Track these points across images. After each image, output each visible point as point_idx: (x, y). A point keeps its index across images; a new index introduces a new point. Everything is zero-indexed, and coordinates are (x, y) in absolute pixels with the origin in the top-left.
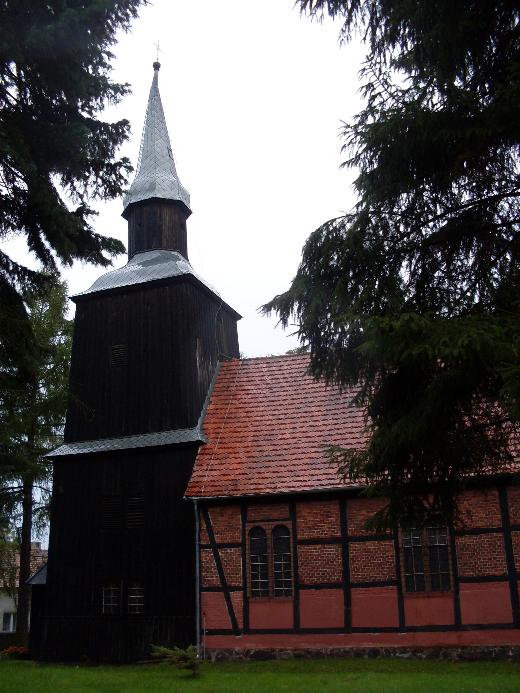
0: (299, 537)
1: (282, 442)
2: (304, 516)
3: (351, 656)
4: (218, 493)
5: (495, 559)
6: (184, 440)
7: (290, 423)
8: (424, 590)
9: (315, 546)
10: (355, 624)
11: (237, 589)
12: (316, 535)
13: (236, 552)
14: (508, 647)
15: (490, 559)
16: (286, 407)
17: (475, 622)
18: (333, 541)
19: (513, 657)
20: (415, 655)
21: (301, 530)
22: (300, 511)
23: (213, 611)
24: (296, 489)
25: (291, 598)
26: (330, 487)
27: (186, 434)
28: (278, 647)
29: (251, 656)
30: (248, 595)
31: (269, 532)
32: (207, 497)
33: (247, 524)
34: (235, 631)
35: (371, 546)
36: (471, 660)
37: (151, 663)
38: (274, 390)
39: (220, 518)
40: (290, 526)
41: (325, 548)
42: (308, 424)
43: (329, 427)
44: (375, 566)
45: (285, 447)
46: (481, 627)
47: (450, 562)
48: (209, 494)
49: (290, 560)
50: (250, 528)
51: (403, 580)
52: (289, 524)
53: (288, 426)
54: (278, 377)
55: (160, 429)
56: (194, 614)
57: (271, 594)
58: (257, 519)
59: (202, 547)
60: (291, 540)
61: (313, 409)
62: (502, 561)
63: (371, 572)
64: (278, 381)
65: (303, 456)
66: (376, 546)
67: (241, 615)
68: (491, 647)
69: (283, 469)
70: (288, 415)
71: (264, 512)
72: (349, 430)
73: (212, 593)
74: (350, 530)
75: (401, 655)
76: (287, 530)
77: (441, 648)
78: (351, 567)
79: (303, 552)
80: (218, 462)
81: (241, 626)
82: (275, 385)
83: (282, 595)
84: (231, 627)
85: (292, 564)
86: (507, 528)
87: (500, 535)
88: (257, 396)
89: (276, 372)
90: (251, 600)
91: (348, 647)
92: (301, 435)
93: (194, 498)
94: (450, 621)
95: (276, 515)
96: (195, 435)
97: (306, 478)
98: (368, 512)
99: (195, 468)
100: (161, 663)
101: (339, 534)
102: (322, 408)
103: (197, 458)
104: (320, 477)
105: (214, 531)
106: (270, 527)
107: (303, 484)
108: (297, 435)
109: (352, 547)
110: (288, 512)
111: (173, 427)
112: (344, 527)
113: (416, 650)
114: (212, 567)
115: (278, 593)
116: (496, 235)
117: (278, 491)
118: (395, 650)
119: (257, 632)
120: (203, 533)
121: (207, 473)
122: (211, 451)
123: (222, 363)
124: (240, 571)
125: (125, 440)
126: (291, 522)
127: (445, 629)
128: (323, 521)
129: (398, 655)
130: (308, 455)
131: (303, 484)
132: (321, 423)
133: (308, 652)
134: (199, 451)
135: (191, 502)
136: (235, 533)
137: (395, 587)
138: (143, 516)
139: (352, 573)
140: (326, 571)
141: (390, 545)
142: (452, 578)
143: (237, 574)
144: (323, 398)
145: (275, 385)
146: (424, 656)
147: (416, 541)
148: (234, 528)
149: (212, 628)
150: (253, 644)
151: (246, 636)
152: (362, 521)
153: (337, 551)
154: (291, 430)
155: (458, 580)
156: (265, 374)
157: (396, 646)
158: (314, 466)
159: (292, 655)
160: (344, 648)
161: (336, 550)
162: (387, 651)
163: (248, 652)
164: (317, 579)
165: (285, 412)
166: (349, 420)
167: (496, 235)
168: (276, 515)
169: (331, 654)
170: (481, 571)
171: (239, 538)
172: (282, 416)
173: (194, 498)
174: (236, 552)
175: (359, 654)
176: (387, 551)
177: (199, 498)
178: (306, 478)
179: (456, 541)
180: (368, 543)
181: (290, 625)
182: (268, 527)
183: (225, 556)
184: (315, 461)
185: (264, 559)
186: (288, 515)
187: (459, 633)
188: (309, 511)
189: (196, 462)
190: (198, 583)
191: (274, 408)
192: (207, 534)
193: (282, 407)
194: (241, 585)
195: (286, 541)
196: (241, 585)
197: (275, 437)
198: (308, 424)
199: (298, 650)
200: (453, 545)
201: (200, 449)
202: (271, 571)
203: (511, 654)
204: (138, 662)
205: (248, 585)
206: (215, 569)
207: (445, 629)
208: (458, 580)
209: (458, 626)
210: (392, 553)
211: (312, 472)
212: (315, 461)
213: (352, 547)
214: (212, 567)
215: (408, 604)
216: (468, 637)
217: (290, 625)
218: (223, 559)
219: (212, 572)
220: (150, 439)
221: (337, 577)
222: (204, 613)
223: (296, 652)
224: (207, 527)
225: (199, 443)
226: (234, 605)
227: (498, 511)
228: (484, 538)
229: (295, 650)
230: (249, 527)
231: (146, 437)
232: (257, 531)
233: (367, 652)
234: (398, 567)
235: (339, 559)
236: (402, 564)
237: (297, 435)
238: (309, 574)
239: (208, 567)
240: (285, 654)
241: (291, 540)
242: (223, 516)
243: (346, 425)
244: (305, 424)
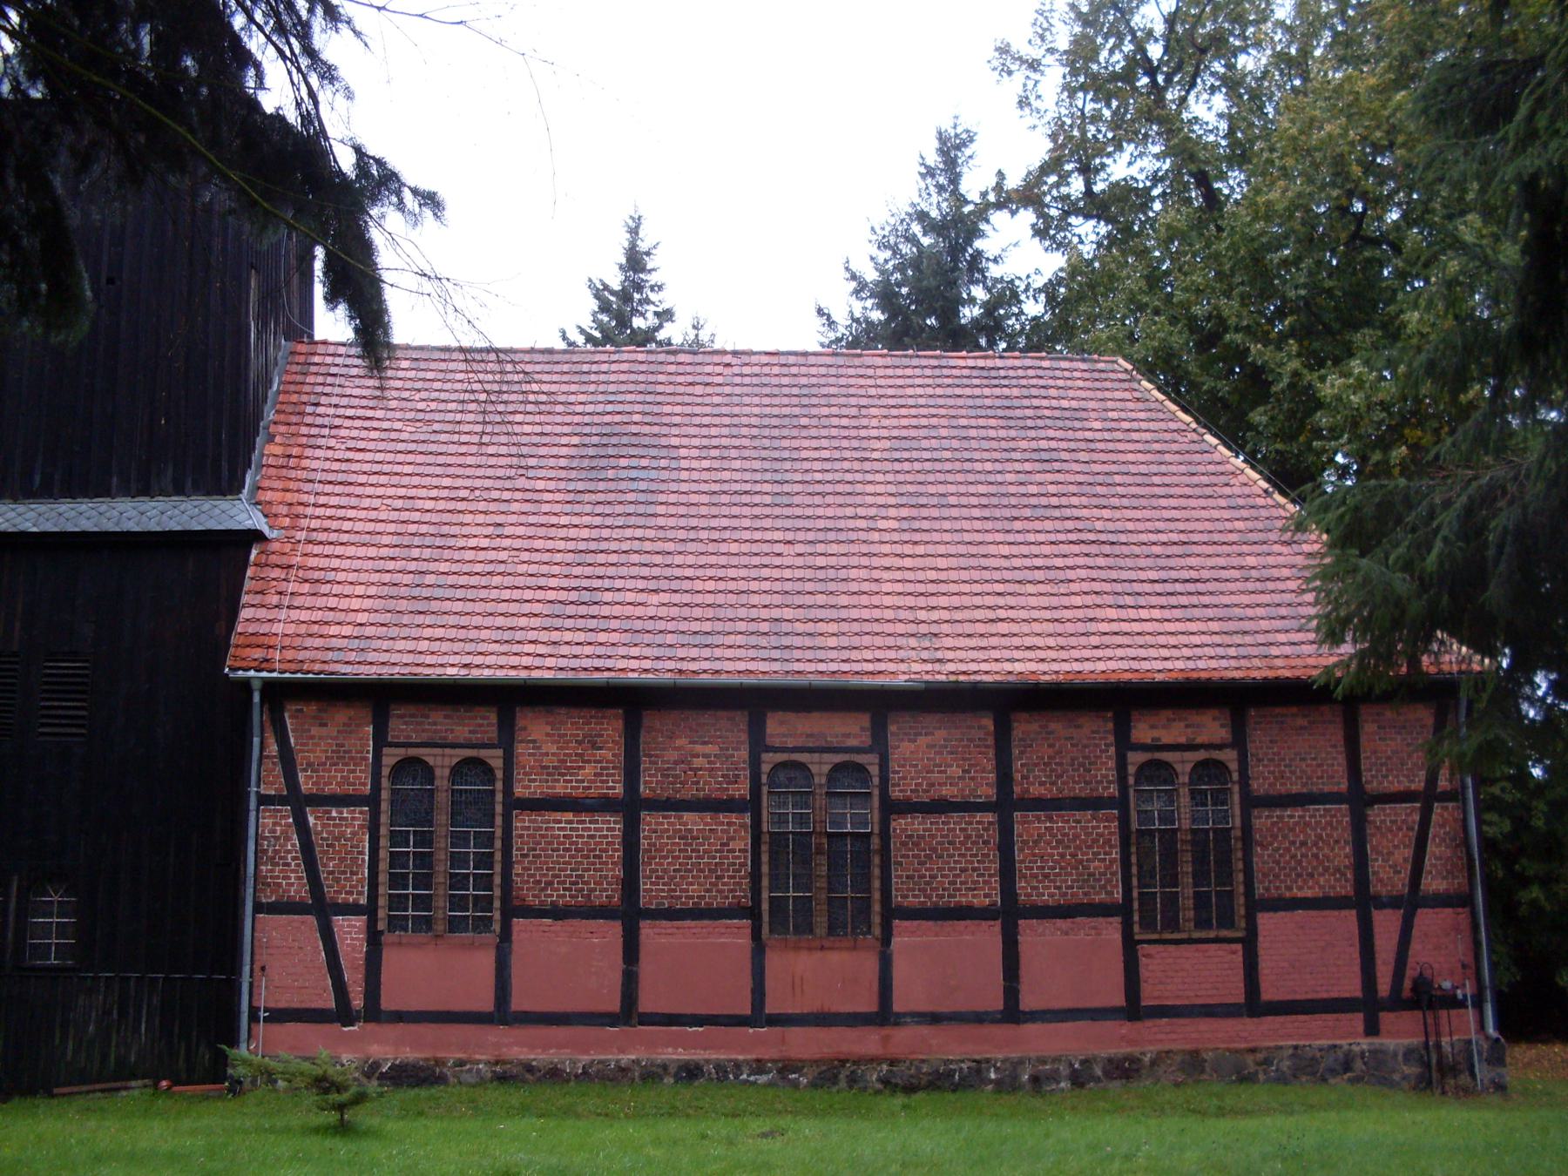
0: (519, 791)
1: (469, 555)
2: (534, 741)
3: (633, 1080)
4: (317, 667)
5: (974, 869)
6: (213, 525)
7: (485, 513)
8: (811, 931)
9: (558, 816)
10: (646, 1004)
11: (353, 909)
12: (560, 789)
13: (353, 819)
14: (988, 1061)
15: (963, 870)
16: (469, 472)
18: (605, 805)
19: (998, 1083)
21: (525, 774)
22: (525, 729)
23: (282, 960)
24: (523, 674)
25: (491, 938)
26: (606, 674)
27: (217, 511)
28: (453, 1056)
29: (382, 1077)
30: (381, 926)
31: (442, 774)
32: (287, 675)
33: (386, 750)
34: (343, 1014)
35: (695, 823)
36: (910, 1089)
37: (94, 1091)
38: (436, 427)
39: (314, 731)
40: (497, 763)
41: (583, 822)
42: (532, 519)
43: (585, 533)
44: (702, 871)
45: (478, 568)
46: (934, 1019)
48: (293, 666)
49: (492, 846)
50: (393, 761)
51: (765, 906)
52: (495, 758)
53: (480, 519)
54: (443, 396)
55: (145, 488)
56: (236, 969)
57: (440, 927)
58: (414, 739)
59: (264, 800)
60: (499, 797)
61: (540, 485)
62: (990, 876)
63: (692, 884)
64: (442, 406)
65: (528, 594)
66: (706, 824)
67: (360, 976)
68: (952, 1062)
69: (477, 620)
70: (477, 493)
71: (435, 724)
72: (636, 545)
73: (283, 918)
74: (646, 782)
75: (752, 1078)
76: (489, 771)
77: (843, 1062)
78: (645, 871)
79: (528, 828)
80: (306, 588)
81: (358, 1002)
82: (438, 417)
83: (466, 931)
84: (332, 1004)
85: (498, 856)
86: (1006, 804)
87: (990, 817)
88: (394, 435)
89: (437, 385)
90: (387, 938)
91: (626, 1058)
92: (518, 543)
93: (252, 673)
94: (868, 1004)
95: (462, 732)
96: (239, 514)
97: (541, 649)
98: (694, 743)
99: (245, 599)
100: (124, 1093)
101: (619, 790)
102: (562, 485)
103: (249, 573)
104: (577, 650)
105: (298, 761)
106: (447, 761)
107: (538, 662)
108: (507, 543)
109: (649, 824)
110: (495, 728)
111: (179, 489)
112: (631, 774)
113: (787, 1067)
114: (289, 852)
115: (454, 925)
117: (475, 673)
118: (738, 1066)
119: (399, 1017)
120: (268, 764)
121: (283, 614)
122: (284, 560)
123: (291, 345)
124: (362, 865)
125: (42, 508)
126: (500, 752)
128: (581, 755)
129: (744, 1076)
130: (540, 595)
131: (538, 662)
132: (564, 520)
133: (529, 1068)
134: (252, 557)
135: (246, 684)
136: (354, 771)
137: (747, 922)
138: (84, 713)
139: (644, 885)
140: (582, 876)
141: (741, 825)
142: (877, 907)
143: (352, 873)
144: (563, 463)
145: (438, 417)
146: (804, 1080)
147: (801, 819)
148: (352, 758)
149: (282, 1005)
150: (388, 1047)
151: (371, 1026)
152: (676, 763)
153: (613, 829)
154: (490, 530)
155: (891, 913)
156: (409, 385)
157: (741, 1057)
158: (558, 623)
159: (489, 1075)
160: (618, 1061)
161: (609, 827)
162: (721, 1068)
164: (554, 896)
165: (468, 483)
166: (632, 521)
168: (462, 732)
169: (585, 1073)
170: (943, 896)
171: (364, 784)
172: (463, 493)
173: (252, 673)
174: (356, 817)
175: (652, 1075)
176: (733, 838)
177: (264, 674)
178: (541, 649)
179: (893, 824)
180: (687, 816)
181: (486, 1003)
182: (442, 762)
183: (324, 826)
184: (558, 609)
185: (425, 839)
186: (495, 735)
187: (887, 1031)
188: (548, 729)
189: (248, 584)
190: (250, 891)
191: (439, 471)
192: (279, 769)
193: (460, 471)
194: (363, 901)
195: (483, 795)
196: (363, 901)
197: (451, 542)
198: (532, 519)
199: (504, 1062)
200: (885, 834)
201: (254, 553)
202: (442, 868)
203: (993, 1076)
204: (56, 1091)
205: (382, 902)
206: (294, 859)
208: (891, 913)
209: (884, 1016)
210: (743, 842)
211: (555, 636)
212: (558, 609)
213: (649, 824)
214: (289, 852)
215: (775, 962)
216: (904, 1039)
217: (486, 1003)
218: (317, 833)
219: (288, 865)
220: (115, 513)
221: (607, 892)
222: (263, 969)
223: (498, 1069)
224: (281, 750)
225: (256, 536)
226: (343, 949)
227: (990, 765)
228: (955, 823)
229: (497, 1063)
230: (391, 757)
231: (103, 508)
232: (411, 767)
233: (672, 1070)
234: (755, 876)
235: (615, 850)
236: (765, 869)
237: (507, 543)
238: (539, 882)
239: (276, 852)
240: (470, 1070)
241: (499, 797)
242: (325, 725)
243: (629, 533)
244: (523, 519)
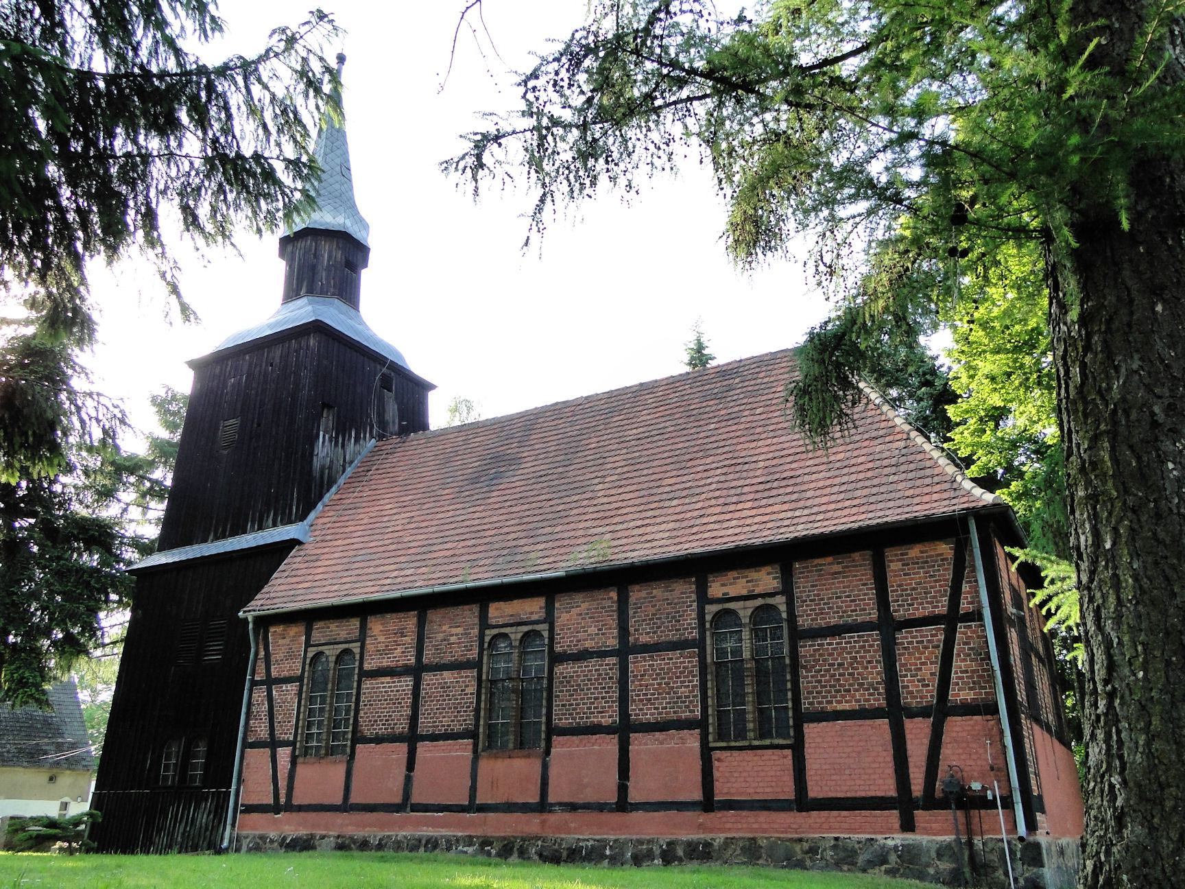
12: (385, 663)
15: (596, 699)
17: (567, 799)
20: (483, 849)
23: (255, 775)
25: (346, 758)
34: (276, 808)
46: (573, 807)
47: (544, 702)
78: (422, 710)
81: (283, 800)
90: (300, 760)
101: (413, 660)
113: (486, 842)
116: (1159, 308)
127: (525, 808)
155: (553, 731)
163: (284, 839)
164: (380, 729)
167: (1159, 308)
187: (545, 816)
194: (291, 739)
207: (525, 808)
210: (472, 689)
229: (338, 837)
236: (483, 705)
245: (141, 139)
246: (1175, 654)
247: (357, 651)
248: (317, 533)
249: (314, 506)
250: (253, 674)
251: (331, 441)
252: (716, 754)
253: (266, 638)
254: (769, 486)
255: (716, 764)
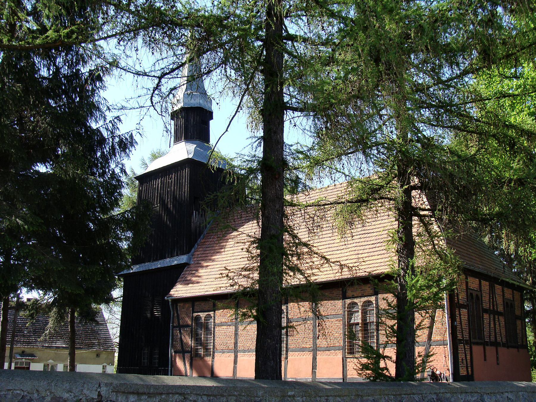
78: (239, 340)
90: (194, 359)
245: (501, 69)
246: (227, 23)
247: (212, 315)
248: (195, 259)
249: (194, 246)
250: (173, 323)
251: (199, 214)
252: (348, 360)
253: (177, 308)
254: (375, 246)
255: (348, 364)
